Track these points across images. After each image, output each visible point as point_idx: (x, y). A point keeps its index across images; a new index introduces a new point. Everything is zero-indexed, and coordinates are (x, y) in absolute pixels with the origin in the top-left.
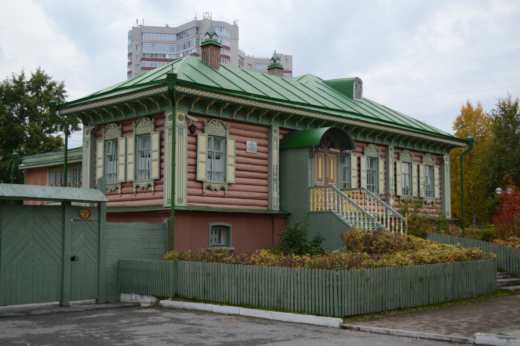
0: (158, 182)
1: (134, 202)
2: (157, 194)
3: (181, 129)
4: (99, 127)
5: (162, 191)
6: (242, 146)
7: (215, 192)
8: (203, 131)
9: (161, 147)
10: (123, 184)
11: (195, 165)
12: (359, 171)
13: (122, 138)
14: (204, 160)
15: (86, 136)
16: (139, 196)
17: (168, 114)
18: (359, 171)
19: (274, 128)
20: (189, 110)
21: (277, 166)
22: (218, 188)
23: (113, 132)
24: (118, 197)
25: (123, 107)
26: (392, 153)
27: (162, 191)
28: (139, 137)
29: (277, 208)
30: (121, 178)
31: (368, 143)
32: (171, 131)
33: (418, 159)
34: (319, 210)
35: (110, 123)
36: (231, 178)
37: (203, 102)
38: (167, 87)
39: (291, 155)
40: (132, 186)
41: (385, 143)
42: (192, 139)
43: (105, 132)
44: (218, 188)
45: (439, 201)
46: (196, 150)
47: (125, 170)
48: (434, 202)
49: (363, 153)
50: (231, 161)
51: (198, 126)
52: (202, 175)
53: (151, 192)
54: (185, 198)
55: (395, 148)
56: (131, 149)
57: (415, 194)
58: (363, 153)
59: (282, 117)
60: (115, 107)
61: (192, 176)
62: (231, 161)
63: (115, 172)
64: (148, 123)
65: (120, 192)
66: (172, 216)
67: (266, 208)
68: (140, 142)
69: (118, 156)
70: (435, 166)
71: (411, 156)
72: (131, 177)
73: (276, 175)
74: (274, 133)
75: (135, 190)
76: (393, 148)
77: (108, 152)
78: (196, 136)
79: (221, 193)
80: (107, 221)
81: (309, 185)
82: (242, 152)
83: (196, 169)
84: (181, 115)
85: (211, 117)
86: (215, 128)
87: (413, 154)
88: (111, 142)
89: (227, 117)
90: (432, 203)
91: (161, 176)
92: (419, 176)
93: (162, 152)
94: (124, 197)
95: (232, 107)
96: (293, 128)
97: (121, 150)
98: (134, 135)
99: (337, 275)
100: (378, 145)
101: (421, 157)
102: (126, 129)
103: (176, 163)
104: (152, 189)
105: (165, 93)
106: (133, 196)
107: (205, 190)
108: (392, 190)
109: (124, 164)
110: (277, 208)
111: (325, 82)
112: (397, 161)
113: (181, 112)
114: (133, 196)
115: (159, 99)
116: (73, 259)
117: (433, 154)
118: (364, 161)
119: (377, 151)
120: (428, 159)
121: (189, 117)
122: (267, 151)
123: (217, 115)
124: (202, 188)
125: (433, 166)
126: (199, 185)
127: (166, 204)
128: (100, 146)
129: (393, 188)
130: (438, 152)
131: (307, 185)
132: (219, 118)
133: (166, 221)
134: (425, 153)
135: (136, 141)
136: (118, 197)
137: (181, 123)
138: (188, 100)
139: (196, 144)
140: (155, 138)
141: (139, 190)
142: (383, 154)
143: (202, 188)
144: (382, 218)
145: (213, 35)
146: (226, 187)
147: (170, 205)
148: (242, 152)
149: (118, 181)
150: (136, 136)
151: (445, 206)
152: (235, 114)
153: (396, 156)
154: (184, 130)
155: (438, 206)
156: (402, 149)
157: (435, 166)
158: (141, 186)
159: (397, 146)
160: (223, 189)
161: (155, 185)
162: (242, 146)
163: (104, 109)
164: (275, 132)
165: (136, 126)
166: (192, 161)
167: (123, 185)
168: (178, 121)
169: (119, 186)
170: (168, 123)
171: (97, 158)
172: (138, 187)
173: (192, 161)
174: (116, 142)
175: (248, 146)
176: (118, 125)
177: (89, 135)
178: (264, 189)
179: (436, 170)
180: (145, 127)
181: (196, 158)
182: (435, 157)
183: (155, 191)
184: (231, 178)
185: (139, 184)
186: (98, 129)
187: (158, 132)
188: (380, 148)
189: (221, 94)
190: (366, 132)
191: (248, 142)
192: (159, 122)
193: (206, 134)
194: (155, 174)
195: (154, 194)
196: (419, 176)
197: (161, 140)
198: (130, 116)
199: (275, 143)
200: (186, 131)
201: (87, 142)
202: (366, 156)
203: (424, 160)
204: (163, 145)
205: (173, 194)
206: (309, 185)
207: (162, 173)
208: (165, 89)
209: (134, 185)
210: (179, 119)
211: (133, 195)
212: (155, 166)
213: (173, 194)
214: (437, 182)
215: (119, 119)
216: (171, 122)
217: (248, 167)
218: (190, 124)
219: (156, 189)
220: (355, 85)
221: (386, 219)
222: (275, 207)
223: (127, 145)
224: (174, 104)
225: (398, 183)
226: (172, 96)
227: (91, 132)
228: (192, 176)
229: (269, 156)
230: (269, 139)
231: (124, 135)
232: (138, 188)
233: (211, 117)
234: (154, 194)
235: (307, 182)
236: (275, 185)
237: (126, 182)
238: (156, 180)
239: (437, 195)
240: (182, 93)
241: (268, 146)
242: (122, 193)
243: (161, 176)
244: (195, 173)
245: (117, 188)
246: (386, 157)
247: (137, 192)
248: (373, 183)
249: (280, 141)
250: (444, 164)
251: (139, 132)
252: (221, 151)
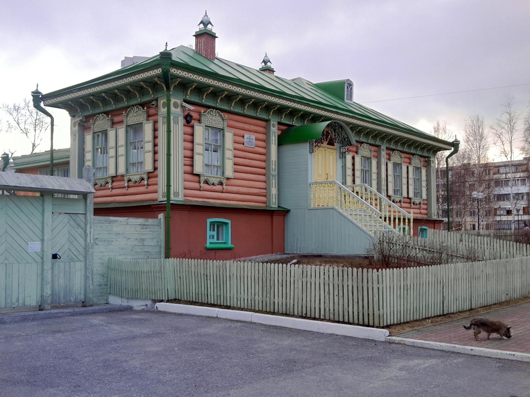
0: (151, 175)
1: (126, 197)
2: (151, 188)
3: (176, 118)
4: (88, 118)
5: (157, 184)
6: (240, 139)
7: (213, 186)
8: (199, 121)
9: (155, 137)
10: (114, 178)
11: (192, 158)
12: (354, 170)
13: (112, 129)
14: (202, 152)
15: (73, 128)
16: (132, 190)
17: (161, 102)
18: (354, 170)
19: (272, 123)
20: (184, 97)
21: (275, 161)
22: (216, 182)
23: (102, 123)
24: (108, 192)
25: (113, 95)
26: (384, 153)
27: (157, 184)
28: (131, 128)
29: (275, 204)
30: (112, 172)
31: (362, 143)
32: (166, 120)
33: (407, 160)
34: (325, 206)
35: (99, 114)
36: (229, 173)
37: (200, 89)
38: (160, 69)
39: (291, 150)
40: (123, 180)
41: (378, 143)
42: (189, 130)
43: (94, 124)
44: (216, 182)
45: (425, 202)
46: (192, 142)
47: (115, 163)
48: (422, 202)
49: (357, 152)
50: (229, 154)
51: (195, 115)
52: (198, 168)
53: (144, 185)
54: (181, 192)
55: (387, 149)
56: (122, 141)
57: (405, 194)
58: (357, 152)
59: (281, 110)
60: (103, 95)
61: (188, 169)
62: (229, 154)
63: (105, 165)
64: (140, 112)
65: (110, 186)
66: (167, 210)
67: (264, 205)
68: (131, 132)
69: (108, 148)
70: (422, 168)
71: (401, 157)
72: (122, 170)
73: (275, 171)
74: (272, 128)
75: (126, 184)
76: (385, 148)
77: (98, 145)
78: (193, 127)
79: (219, 188)
80: (94, 215)
81: (310, 181)
82: (240, 146)
83: (193, 161)
84: (176, 102)
85: (209, 107)
86: (213, 119)
87: (403, 155)
88: (100, 134)
89: (225, 107)
90: (420, 204)
91: (155, 169)
92: (408, 177)
93: (156, 143)
94: (115, 191)
95: (230, 97)
96: (291, 123)
97: (111, 142)
98: (124, 126)
100: (371, 145)
101: (410, 159)
102: (116, 119)
103: (172, 153)
104: (146, 183)
105: (158, 76)
106: (124, 191)
107: (202, 184)
108: (384, 190)
109: (115, 157)
110: (275, 204)
111: (314, 85)
112: (388, 162)
113: (176, 100)
114: (124, 191)
115: (153, 85)
116: (55, 256)
117: (421, 156)
118: (358, 159)
119: (370, 151)
120: (416, 161)
121: (185, 104)
122: (265, 146)
123: (214, 105)
124: (199, 182)
125: (420, 168)
126: (196, 178)
127: (161, 197)
128: (89, 138)
129: (385, 188)
130: (425, 154)
131: (307, 181)
132: (217, 109)
133: (161, 216)
134: (413, 155)
135: (127, 132)
136: (108, 192)
137: (176, 111)
138: (184, 85)
139: (192, 135)
140: (148, 127)
141: (131, 184)
142: (375, 154)
143: (199, 182)
144: (390, 218)
145: (207, 25)
146: (224, 181)
147: (165, 199)
148: (240, 146)
149: (108, 176)
150: (127, 126)
151: (431, 207)
152: (233, 105)
153: (388, 157)
154: (180, 118)
155: (425, 207)
156: (393, 150)
157: (422, 168)
158: (133, 180)
159: (389, 146)
160: (221, 184)
161: (149, 178)
162: (240, 139)
163: (92, 98)
164: (274, 126)
165: (127, 116)
166: (189, 153)
168: (172, 108)
169: (110, 180)
170: (163, 111)
171: (85, 152)
172: (129, 181)
173: (189, 153)
174: (105, 133)
175: (245, 140)
176: (108, 115)
177: (77, 128)
178: (262, 185)
179: (424, 171)
180: (136, 116)
181: (192, 150)
182: (422, 159)
183: (148, 185)
184: (229, 173)
185: (131, 177)
186: (86, 121)
187: (152, 121)
188: (373, 148)
190: (359, 130)
191: (246, 136)
192: (152, 111)
193: (203, 124)
194: (149, 167)
195: (147, 188)
196: (408, 177)
197: (155, 130)
198: (121, 105)
199: (274, 138)
200: (181, 121)
201: (75, 135)
203: (412, 162)
204: (156, 135)
205: (169, 186)
206: (310, 181)
207: (156, 165)
208: (159, 71)
209: (126, 179)
210: (176, 105)
211: (125, 189)
212: (149, 158)
213: (169, 186)
214: (424, 184)
215: (109, 108)
216: (166, 109)
217: (247, 162)
218: (186, 113)
219: (150, 183)
220: (346, 87)
221: (395, 219)
222: (274, 205)
223: (118, 136)
224: (168, 88)
225: (389, 184)
226: (167, 79)
227: (79, 124)
228: (188, 169)
229: (267, 151)
230: (267, 133)
231: (114, 126)
232: (130, 182)
233: (209, 107)
234: (147, 188)
235: (307, 179)
236: (274, 181)
237: (116, 176)
238: (149, 173)
239: (424, 196)
240: (177, 77)
241: (267, 141)
242: (112, 188)
243: (155, 169)
244: (192, 166)
245: (107, 183)
246: (378, 157)
247: (128, 187)
249: (278, 136)
250: (431, 166)
251: (130, 123)
252: (219, 144)
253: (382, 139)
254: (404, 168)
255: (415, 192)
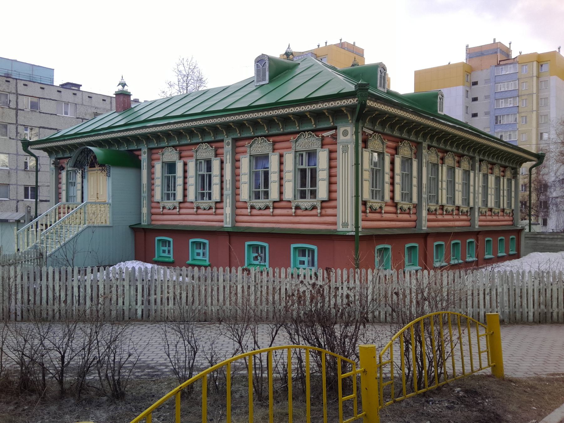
2: (219, 211)
5: (335, 207)
27: (335, 207)
41: (420, 140)
99: (35, 289)
120: (405, 151)
150: (163, 162)
158: (167, 207)
167: (325, 204)
172: (164, 208)
173: (333, 179)
179: (513, 182)
185: (166, 204)
189: (311, 104)
202: (400, 156)
209: (161, 205)
239: (415, 200)
248: (376, 188)
253: (425, 137)
254: (502, 180)
255: (373, 191)
